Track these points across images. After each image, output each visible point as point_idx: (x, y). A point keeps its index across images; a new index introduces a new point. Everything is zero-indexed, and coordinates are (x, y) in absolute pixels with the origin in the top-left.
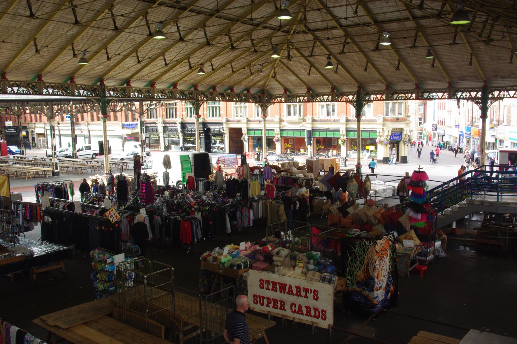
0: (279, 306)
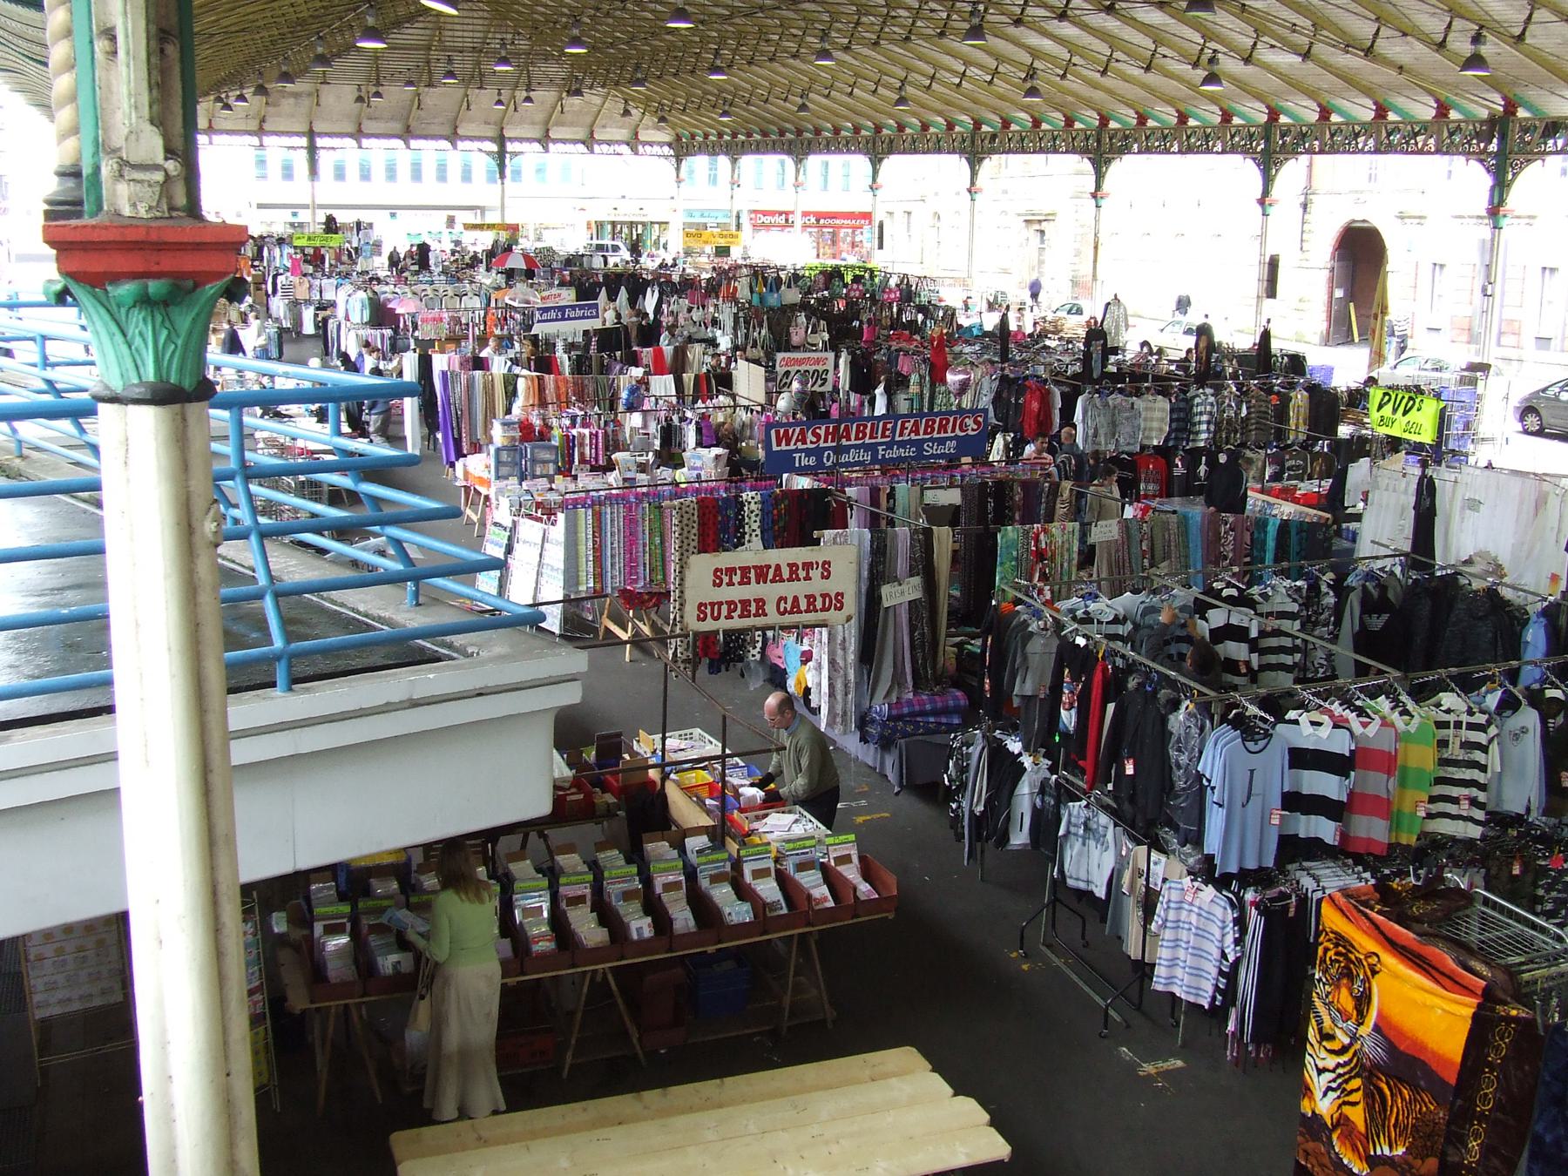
0: (753, 611)
